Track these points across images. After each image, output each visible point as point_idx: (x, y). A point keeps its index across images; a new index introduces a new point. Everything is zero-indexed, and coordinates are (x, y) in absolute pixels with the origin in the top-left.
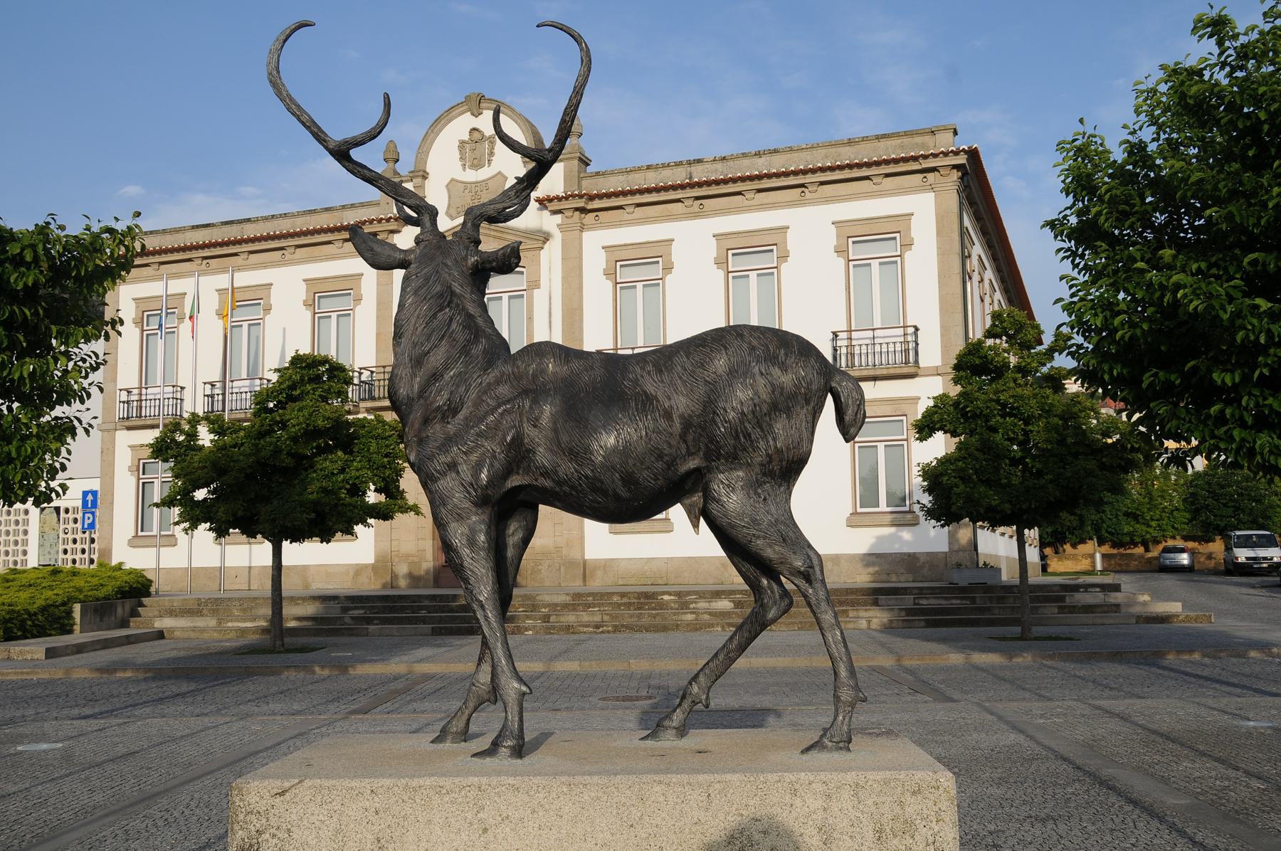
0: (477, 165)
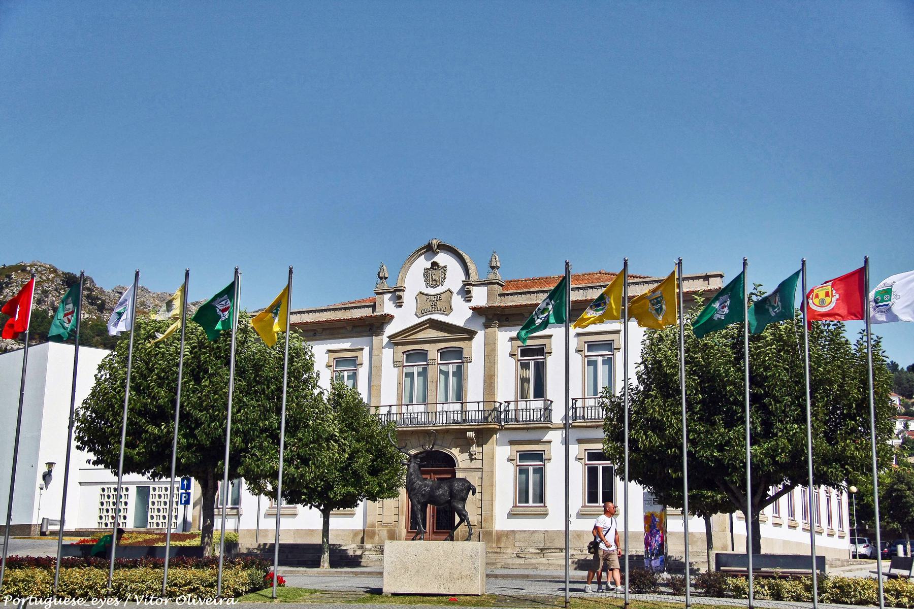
0: (434, 286)
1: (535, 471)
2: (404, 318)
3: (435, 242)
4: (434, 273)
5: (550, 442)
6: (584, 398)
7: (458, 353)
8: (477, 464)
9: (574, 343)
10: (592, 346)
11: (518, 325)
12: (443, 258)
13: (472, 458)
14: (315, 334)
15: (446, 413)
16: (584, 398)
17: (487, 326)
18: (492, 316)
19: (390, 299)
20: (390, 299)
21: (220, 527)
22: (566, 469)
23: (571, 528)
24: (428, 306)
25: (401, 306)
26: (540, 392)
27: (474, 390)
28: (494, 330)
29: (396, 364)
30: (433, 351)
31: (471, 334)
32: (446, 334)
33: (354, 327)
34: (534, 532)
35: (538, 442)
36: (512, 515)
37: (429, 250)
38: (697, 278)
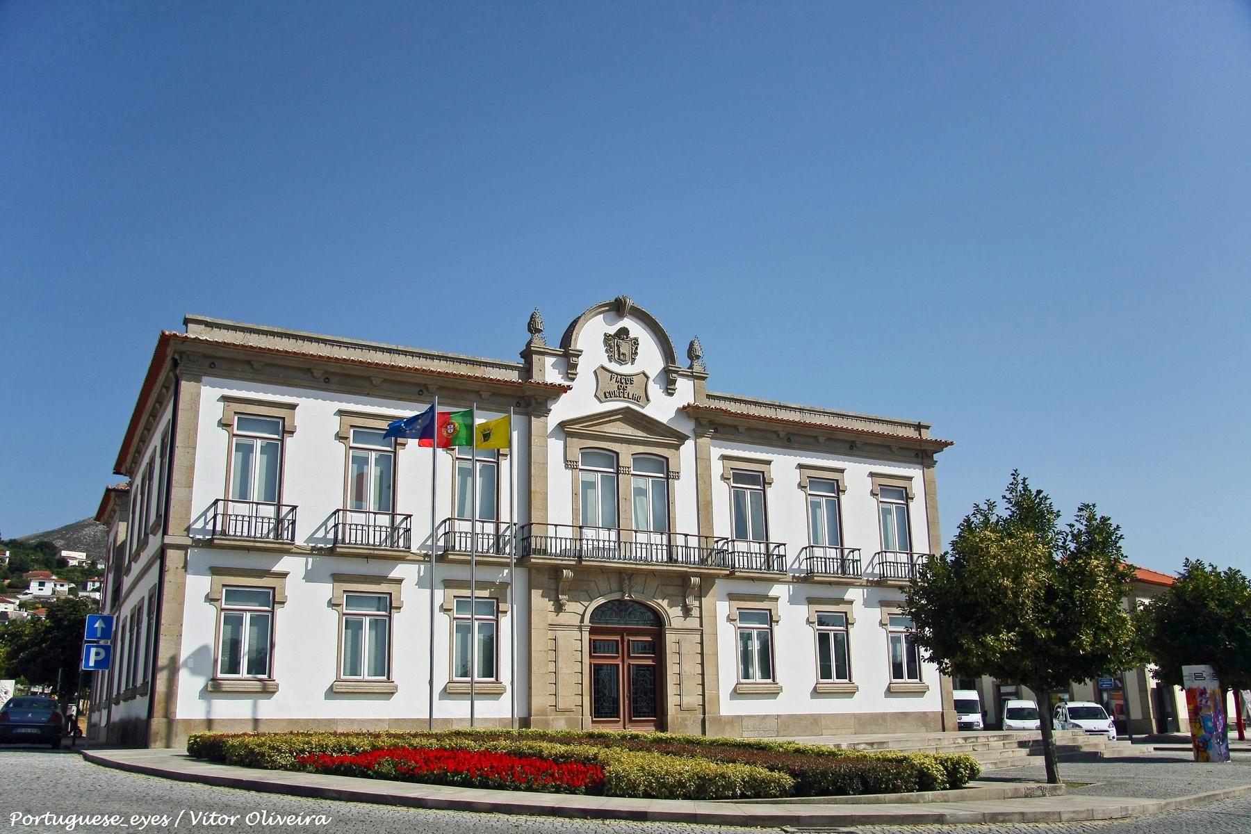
0: (621, 361)
1: (253, 621)
2: (579, 401)
3: (630, 302)
4: (618, 344)
5: (777, 599)
6: (226, 500)
7: (663, 465)
8: (693, 623)
9: (717, 468)
10: (246, 421)
11: (425, 402)
12: (636, 329)
13: (687, 612)
14: (851, 448)
15: (646, 546)
16: (226, 500)
17: (698, 435)
18: (710, 422)
19: (554, 366)
20: (554, 366)
21: (692, 699)
22: (872, 636)
23: (476, 716)
24: (614, 387)
25: (672, 394)
26: (387, 502)
27: (685, 520)
28: (704, 441)
29: (569, 464)
30: (626, 454)
31: (682, 438)
32: (640, 433)
33: (494, 394)
34: (765, 717)
35: (265, 573)
36: (737, 694)
37: (618, 308)
38: (909, 425)
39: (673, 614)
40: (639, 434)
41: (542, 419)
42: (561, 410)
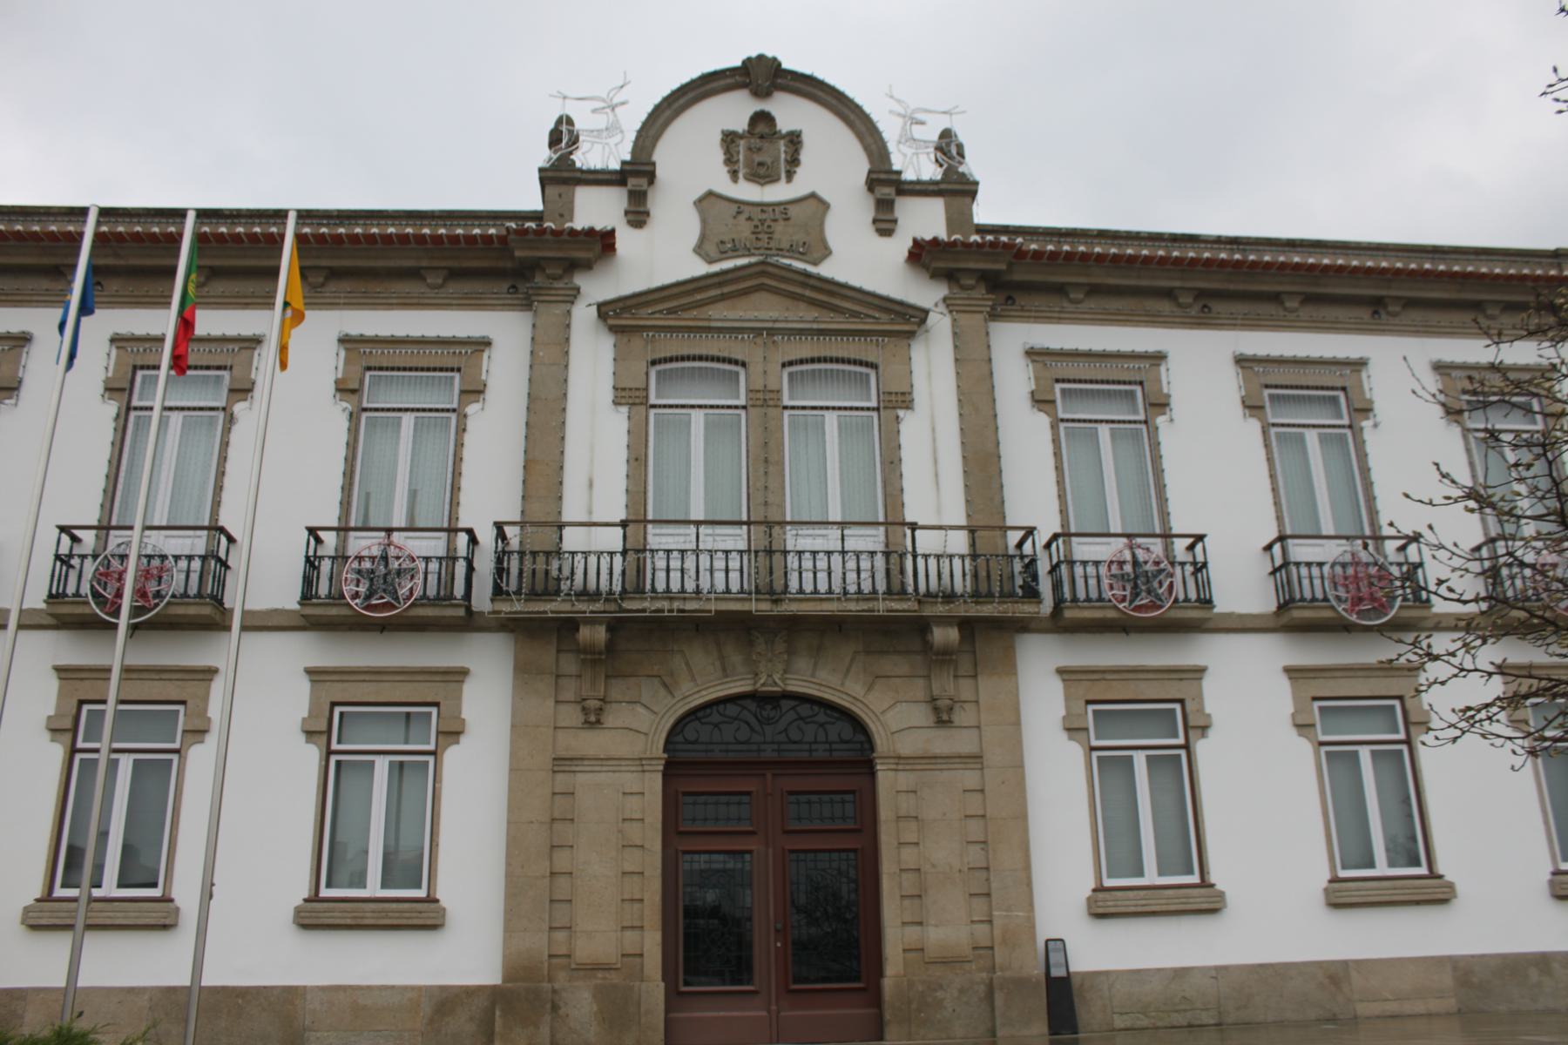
0: (762, 174)
39: (894, 714)
40: (804, 316)
41: (558, 310)
42: (597, 288)
